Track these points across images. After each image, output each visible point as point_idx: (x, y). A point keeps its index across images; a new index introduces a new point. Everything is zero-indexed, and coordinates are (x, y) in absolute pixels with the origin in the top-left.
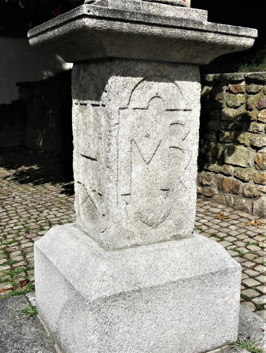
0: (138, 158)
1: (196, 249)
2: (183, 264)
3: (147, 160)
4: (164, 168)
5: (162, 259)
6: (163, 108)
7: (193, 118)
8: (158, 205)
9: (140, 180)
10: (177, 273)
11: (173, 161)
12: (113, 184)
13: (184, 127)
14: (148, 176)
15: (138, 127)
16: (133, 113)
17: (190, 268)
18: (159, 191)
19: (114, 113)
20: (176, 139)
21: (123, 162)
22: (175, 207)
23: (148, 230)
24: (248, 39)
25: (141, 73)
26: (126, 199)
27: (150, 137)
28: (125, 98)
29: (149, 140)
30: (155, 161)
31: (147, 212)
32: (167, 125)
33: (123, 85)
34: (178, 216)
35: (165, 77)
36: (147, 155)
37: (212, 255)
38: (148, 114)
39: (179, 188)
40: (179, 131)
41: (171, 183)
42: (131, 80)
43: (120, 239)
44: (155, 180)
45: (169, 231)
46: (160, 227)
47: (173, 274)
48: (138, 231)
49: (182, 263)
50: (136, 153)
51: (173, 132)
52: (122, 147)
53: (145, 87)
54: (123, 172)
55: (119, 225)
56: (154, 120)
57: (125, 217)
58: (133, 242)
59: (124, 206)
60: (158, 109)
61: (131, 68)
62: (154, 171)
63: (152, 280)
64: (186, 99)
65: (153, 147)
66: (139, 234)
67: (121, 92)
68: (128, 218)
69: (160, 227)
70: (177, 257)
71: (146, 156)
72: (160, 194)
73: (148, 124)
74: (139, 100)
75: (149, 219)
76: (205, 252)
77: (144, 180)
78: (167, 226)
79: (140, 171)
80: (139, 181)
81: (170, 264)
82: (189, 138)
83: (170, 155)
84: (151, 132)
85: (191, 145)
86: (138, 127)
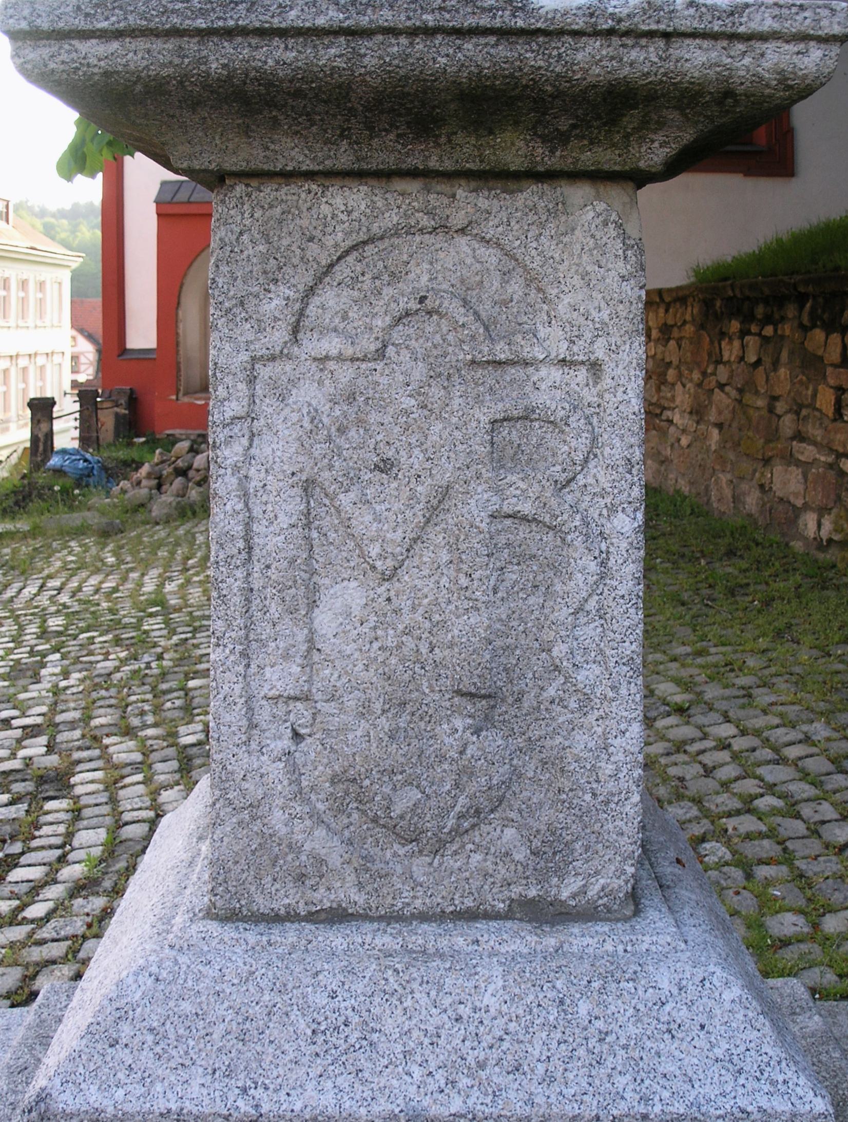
0: (344, 554)
1: (596, 985)
2: (505, 1045)
3: (379, 564)
4: (467, 604)
5: (408, 1003)
6: (455, 354)
7: (607, 396)
8: (442, 758)
9: (353, 646)
10: (464, 1082)
11: (514, 577)
12: (227, 651)
13: (562, 432)
14: (391, 632)
15: (342, 430)
16: (316, 378)
17: (541, 1068)
18: (447, 696)
19: (228, 380)
20: (523, 485)
21: (273, 567)
22: (531, 774)
23: (395, 855)
24: (801, 46)
25: (343, 223)
26: (292, 717)
27: (395, 470)
28: (276, 319)
29: (394, 485)
30: (426, 572)
31: (386, 779)
32: (474, 424)
33: (265, 272)
34: (547, 815)
35: (462, 231)
36: (378, 545)
37: (674, 1026)
38: (384, 380)
39: (551, 692)
40: (542, 450)
41: (505, 670)
42: (298, 251)
43: (258, 878)
44: (424, 650)
45: (500, 877)
46: (456, 853)
47: (443, 1082)
48: (346, 856)
49: (501, 1040)
50: (332, 535)
51: (510, 452)
52: (270, 507)
53: (368, 276)
54: (274, 609)
55: (254, 818)
56: (413, 402)
57: (283, 787)
58: (324, 898)
59: (286, 743)
60: (431, 360)
61: (298, 208)
62: (421, 611)
63: (329, 1084)
64: (565, 317)
65: (409, 514)
66: (349, 869)
67: (257, 296)
68: (299, 794)
69: (456, 853)
70: (485, 1002)
71: (374, 550)
72: (455, 710)
73: (387, 419)
74: (342, 326)
75: (398, 812)
76: (641, 1006)
77: (376, 645)
78: (493, 850)
79: (356, 611)
80: (348, 650)
81: (443, 1032)
82: (591, 480)
83: (500, 551)
84: (402, 453)
85: (605, 512)
86: (342, 430)
